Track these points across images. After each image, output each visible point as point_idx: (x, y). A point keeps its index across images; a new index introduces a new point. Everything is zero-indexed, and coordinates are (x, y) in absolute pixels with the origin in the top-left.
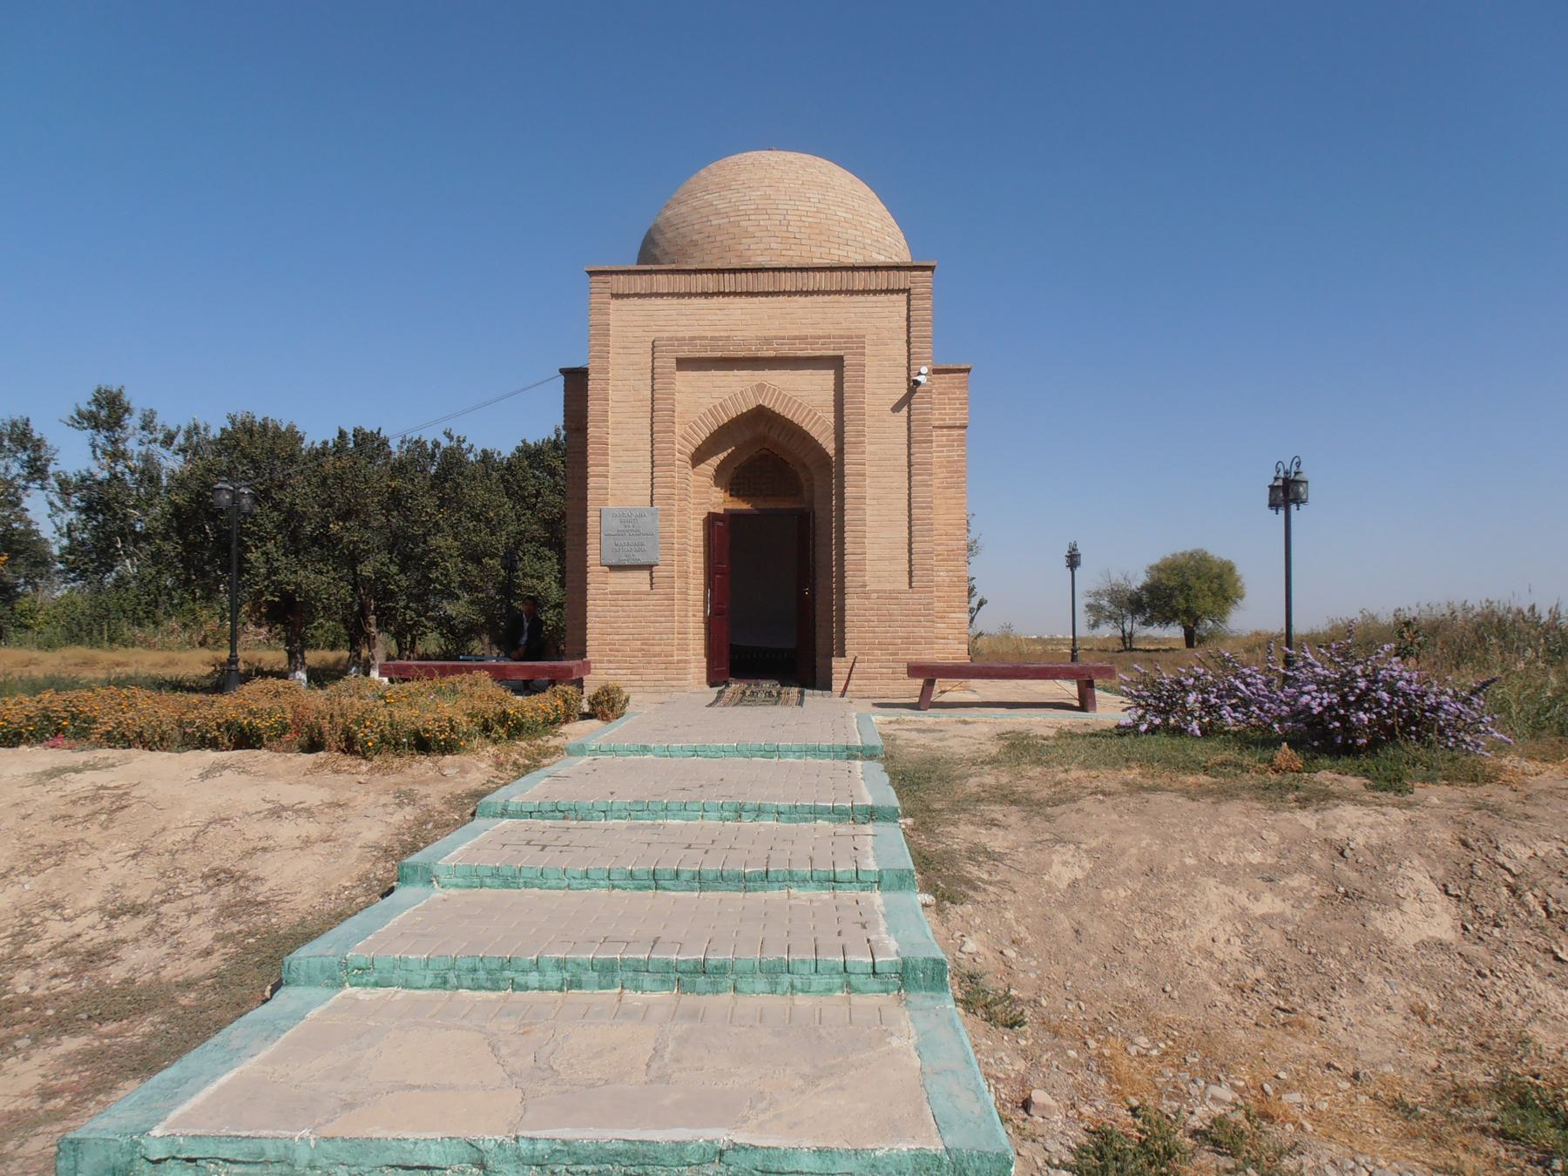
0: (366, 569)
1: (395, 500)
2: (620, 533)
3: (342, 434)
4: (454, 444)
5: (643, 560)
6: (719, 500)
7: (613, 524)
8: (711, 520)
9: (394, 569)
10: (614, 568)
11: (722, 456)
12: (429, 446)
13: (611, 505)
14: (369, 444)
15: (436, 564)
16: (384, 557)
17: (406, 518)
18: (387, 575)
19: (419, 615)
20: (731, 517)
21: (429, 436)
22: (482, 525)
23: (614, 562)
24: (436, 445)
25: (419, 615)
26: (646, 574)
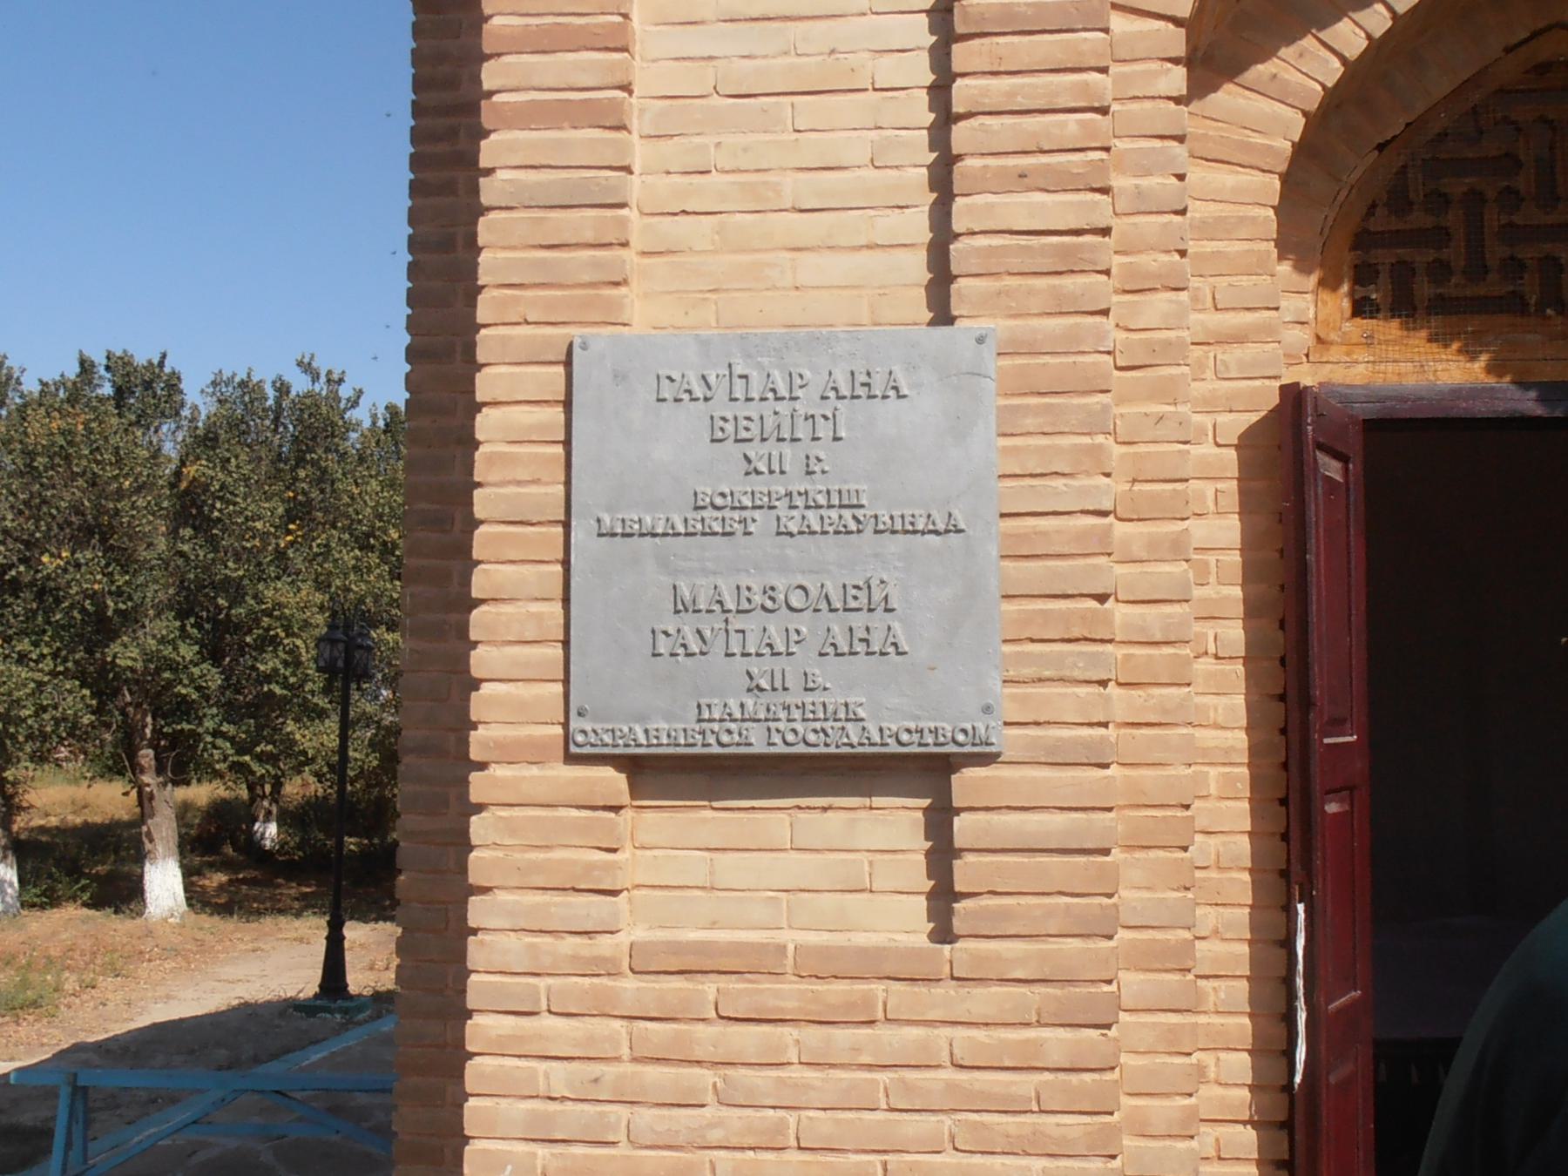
0: (125, 654)
1: (190, 507)
2: (714, 520)
3: (86, 366)
4: (321, 387)
5: (886, 716)
6: (1296, 334)
7: (653, 453)
8: (1288, 438)
9: (188, 651)
10: (658, 774)
11: (1351, 35)
12: (271, 393)
13: (643, 309)
14: (143, 390)
15: (275, 642)
16: (166, 625)
17: (213, 543)
18: (173, 666)
19: (241, 751)
20: (1397, 438)
21: (265, 375)
22: (374, 558)
23: (667, 729)
24: (282, 389)
25: (241, 751)
26: (896, 822)
